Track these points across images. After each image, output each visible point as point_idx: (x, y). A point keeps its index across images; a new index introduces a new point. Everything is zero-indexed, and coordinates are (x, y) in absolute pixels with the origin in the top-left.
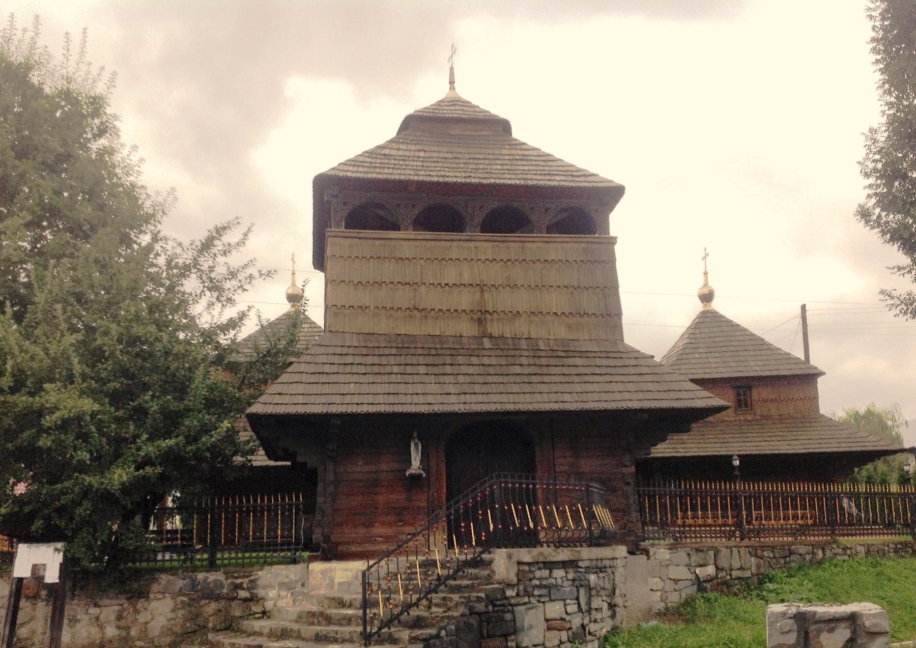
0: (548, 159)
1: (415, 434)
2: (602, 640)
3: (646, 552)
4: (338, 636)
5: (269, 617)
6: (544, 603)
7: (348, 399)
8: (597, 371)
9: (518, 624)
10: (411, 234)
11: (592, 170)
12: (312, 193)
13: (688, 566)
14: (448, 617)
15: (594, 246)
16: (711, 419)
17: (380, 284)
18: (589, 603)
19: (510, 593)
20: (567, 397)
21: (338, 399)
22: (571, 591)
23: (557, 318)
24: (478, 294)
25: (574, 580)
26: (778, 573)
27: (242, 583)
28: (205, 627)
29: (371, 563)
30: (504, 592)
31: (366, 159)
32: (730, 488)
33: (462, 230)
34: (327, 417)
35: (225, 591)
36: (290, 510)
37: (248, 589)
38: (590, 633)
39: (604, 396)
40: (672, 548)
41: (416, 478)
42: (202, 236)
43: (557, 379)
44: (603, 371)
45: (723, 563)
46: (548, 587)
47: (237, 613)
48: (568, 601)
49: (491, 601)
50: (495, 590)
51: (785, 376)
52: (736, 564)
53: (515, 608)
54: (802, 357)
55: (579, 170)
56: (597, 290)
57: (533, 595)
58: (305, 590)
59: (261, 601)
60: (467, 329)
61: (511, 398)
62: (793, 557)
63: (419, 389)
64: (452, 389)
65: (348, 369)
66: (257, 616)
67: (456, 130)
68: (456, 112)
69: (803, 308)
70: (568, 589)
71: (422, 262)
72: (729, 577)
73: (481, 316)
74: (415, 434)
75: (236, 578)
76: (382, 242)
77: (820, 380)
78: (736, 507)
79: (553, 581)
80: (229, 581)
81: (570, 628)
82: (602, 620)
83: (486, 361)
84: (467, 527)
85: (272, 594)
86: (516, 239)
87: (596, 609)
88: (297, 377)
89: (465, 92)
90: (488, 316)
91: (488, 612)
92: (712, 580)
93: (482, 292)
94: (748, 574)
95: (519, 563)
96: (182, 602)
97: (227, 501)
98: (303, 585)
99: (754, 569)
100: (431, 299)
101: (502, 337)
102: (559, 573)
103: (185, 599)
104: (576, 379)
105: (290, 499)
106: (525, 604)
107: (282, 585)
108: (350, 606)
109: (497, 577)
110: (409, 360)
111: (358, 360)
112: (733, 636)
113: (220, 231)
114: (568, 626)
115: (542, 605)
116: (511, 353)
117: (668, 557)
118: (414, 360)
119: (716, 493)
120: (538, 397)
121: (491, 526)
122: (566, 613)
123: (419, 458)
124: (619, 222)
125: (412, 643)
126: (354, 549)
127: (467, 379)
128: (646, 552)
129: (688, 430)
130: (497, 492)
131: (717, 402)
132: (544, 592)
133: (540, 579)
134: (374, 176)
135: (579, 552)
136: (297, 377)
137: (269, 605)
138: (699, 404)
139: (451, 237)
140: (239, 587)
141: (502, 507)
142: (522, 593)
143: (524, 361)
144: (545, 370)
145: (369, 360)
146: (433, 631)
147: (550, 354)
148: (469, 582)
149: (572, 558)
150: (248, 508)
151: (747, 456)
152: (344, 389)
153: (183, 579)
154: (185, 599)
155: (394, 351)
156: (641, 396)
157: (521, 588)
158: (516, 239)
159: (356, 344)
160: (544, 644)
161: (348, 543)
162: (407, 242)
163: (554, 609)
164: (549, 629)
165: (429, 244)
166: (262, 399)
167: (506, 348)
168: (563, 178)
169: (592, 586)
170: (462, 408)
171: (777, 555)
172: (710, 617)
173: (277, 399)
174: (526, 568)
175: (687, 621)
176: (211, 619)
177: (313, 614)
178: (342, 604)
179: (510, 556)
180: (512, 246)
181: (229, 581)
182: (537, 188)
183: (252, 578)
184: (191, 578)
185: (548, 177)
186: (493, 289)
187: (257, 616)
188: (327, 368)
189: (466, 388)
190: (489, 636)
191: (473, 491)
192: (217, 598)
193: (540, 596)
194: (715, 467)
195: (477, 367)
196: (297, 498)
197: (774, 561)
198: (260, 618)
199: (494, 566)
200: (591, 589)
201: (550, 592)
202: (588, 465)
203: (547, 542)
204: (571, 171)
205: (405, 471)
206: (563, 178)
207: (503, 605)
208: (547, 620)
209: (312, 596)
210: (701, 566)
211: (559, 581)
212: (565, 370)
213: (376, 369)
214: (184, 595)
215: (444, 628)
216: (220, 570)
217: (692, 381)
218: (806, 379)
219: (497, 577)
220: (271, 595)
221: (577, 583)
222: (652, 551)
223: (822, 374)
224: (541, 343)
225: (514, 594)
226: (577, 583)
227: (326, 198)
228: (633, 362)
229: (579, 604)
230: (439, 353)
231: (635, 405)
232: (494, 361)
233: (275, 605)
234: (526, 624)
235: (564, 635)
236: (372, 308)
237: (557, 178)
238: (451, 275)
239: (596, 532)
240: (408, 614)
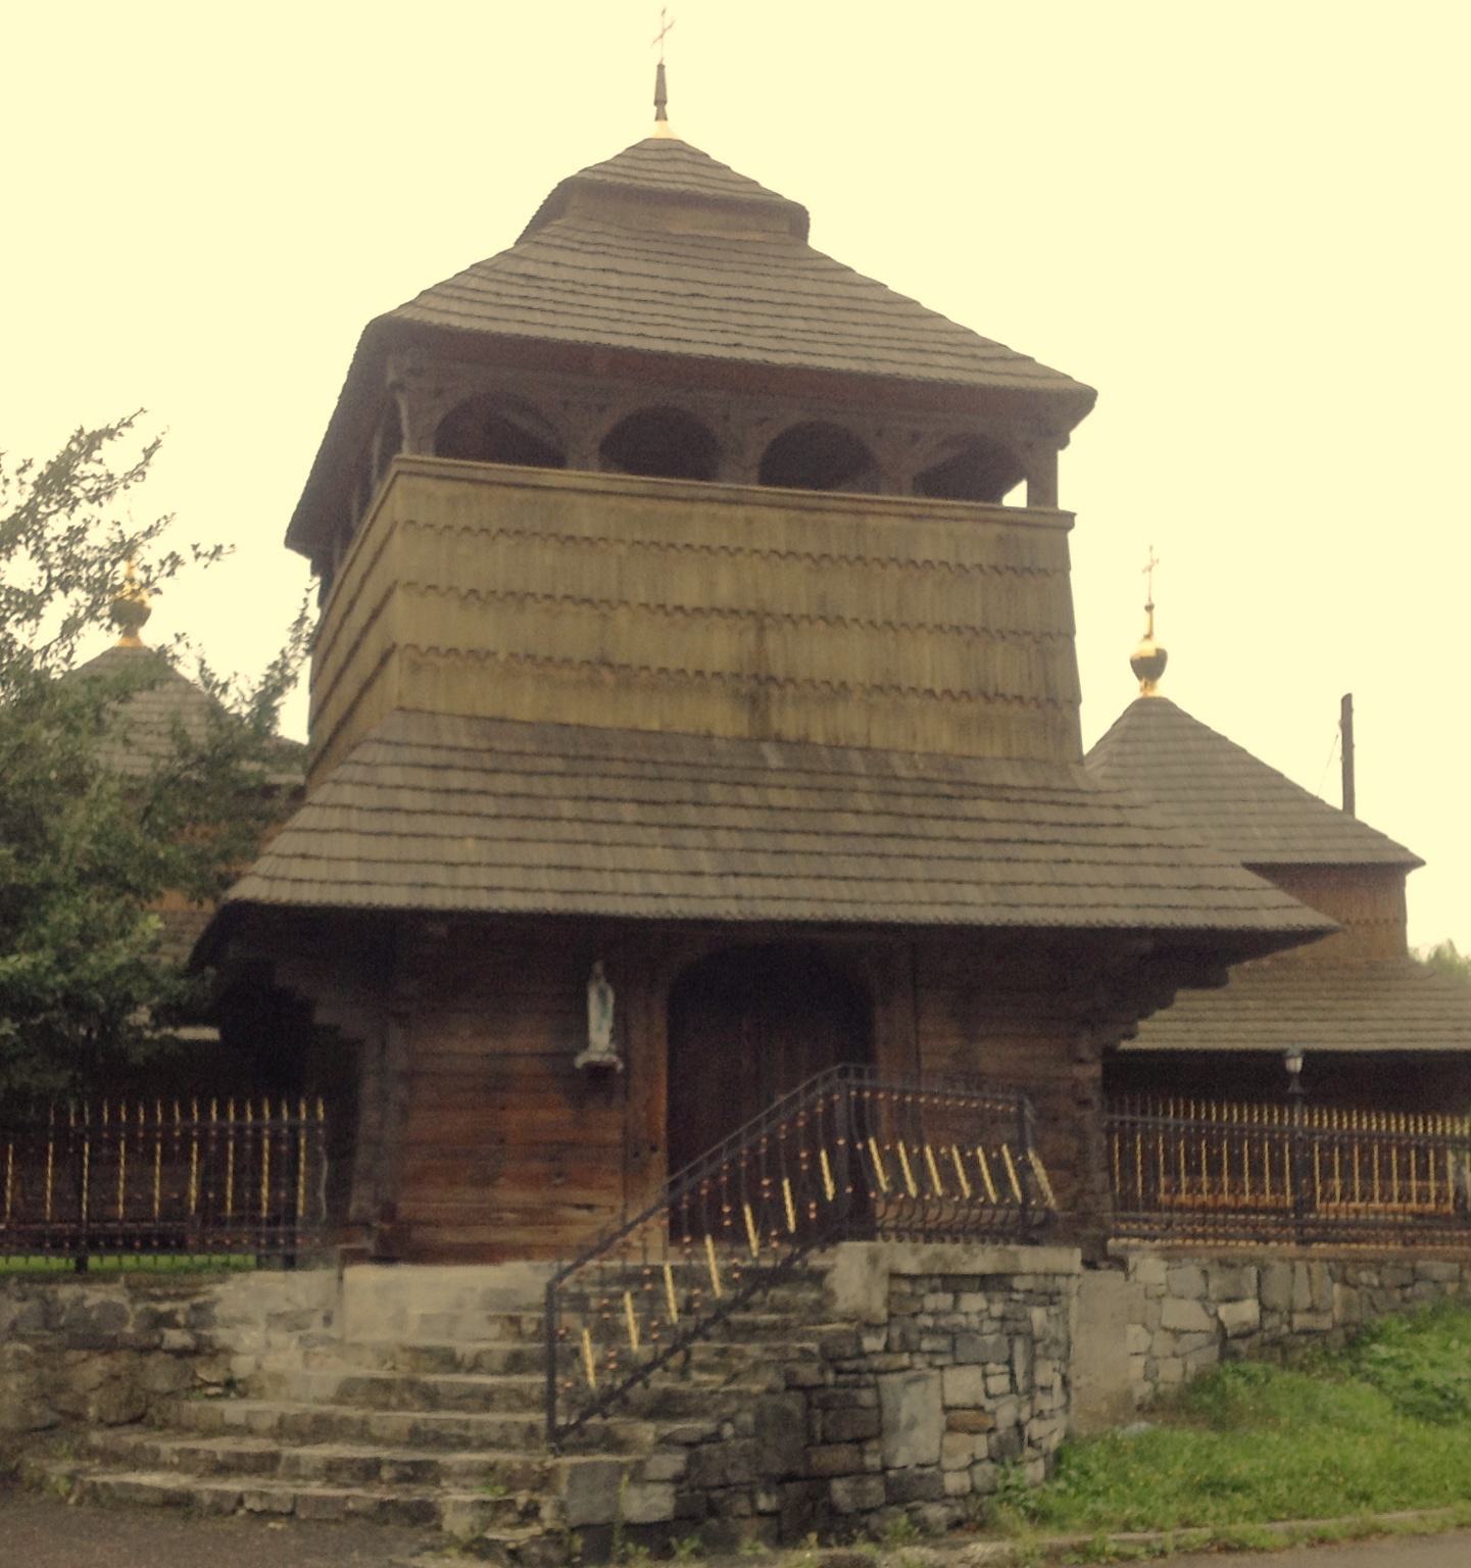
0: (906, 311)
1: (598, 967)
2: (1051, 1459)
3: (1120, 1263)
4: (471, 1433)
5: (243, 1395)
6: (941, 1368)
7: (465, 876)
8: (1033, 833)
9: (887, 1415)
10: (595, 479)
11: (1018, 347)
13: (1203, 1299)
14: (739, 1394)
15: (1022, 532)
16: (1286, 954)
17: (520, 598)
18: (1030, 1373)
19: (871, 1343)
20: (970, 893)
21: (440, 875)
22: (997, 1344)
23: (934, 702)
24: (751, 637)
25: (1003, 1319)
26: (1396, 1326)
27: (171, 1314)
28: (78, 1417)
29: (567, 1263)
30: (859, 1343)
31: (485, 285)
32: (1340, 1124)
33: (704, 474)
34: (421, 915)
35: (129, 1329)
36: (222, 1142)
37: (190, 1327)
38: (1031, 1443)
39: (1055, 895)
40: (1170, 1256)
41: (599, 1073)
42: (46, 451)
43: (944, 848)
44: (1049, 833)
45: (1276, 1297)
46: (952, 1334)
47: (162, 1384)
48: (991, 1367)
49: (832, 1360)
50: (840, 1335)
51: (1334, 866)
52: (1303, 1300)
53: (882, 1379)
54: (1335, 800)
56: (1027, 640)
57: (919, 1350)
58: (333, 1332)
59: (222, 1357)
60: (722, 718)
61: (844, 890)
62: (1421, 1287)
63: (629, 858)
64: (705, 861)
65: (456, 803)
66: (212, 1391)
67: (683, 224)
70: (991, 1339)
71: (622, 549)
72: (1285, 1329)
73: (757, 688)
74: (598, 967)
76: (528, 494)
78: (1303, 1169)
79: (961, 1319)
80: (140, 1307)
81: (992, 1430)
83: (775, 797)
84: (777, 1188)
86: (845, 505)
87: (1043, 1389)
88: (335, 819)
89: (688, 127)
90: (775, 691)
91: (823, 1386)
92: (1250, 1334)
93: (761, 629)
94: (1325, 1323)
95: (895, 1276)
96: (18, 1355)
97: (132, 1112)
98: (327, 1320)
99: (1338, 1313)
100: (641, 642)
101: (804, 742)
102: (973, 1302)
103: (26, 1348)
104: (987, 851)
106: (903, 1369)
107: (275, 1319)
108: (476, 1366)
109: (841, 1306)
110: (597, 787)
111: (476, 781)
112: (1336, 1458)
113: (89, 443)
115: (935, 1373)
116: (828, 780)
117: (1162, 1277)
118: (612, 787)
119: (1282, 1133)
120: (906, 891)
122: (988, 1396)
123: (607, 1024)
124: (1081, 468)
125: (664, 1451)
126: (449, 1237)
127: (738, 841)
128: (1120, 1263)
129: (1219, 982)
130: (840, 1112)
131: (1306, 917)
132: (942, 1343)
133: (934, 1314)
135: (1015, 1254)
136: (335, 819)
137: (242, 1366)
138: (1270, 920)
139: (693, 492)
140: (167, 1320)
141: (851, 1144)
142: (896, 1345)
143: (864, 802)
144: (915, 827)
145: (502, 783)
146: (705, 1426)
147: (921, 787)
148: (774, 1317)
149: (1001, 1268)
150: (222, 1131)
151: (1325, 1054)
152: (453, 851)
153: (18, 1299)
154: (26, 1348)
155: (558, 764)
156: (1139, 896)
157: (896, 1332)
158: (845, 505)
159: (465, 742)
161: (437, 1224)
162: (585, 499)
163: (962, 1385)
164: (951, 1428)
165: (638, 506)
166: (264, 865)
167: (822, 769)
168: (956, 362)
169: (1037, 1332)
170: (729, 910)
171: (1388, 1282)
172: (1268, 1417)
173: (298, 869)
174: (906, 1287)
175: (1218, 1424)
176: (93, 1397)
177: (387, 1386)
178: (449, 1361)
179: (873, 1260)
180: (838, 520)
181: (140, 1307)
182: (895, 381)
183: (199, 1300)
184: (41, 1296)
185: (922, 358)
186: (788, 626)
187: (212, 1391)
188: (406, 799)
189: (739, 863)
190: (826, 1442)
192: (109, 1347)
193: (933, 1352)
194: (1250, 1076)
195: (756, 813)
197: (1381, 1293)
198: (217, 1396)
199: (834, 1281)
200: (1034, 1342)
201: (956, 1345)
202: (996, 1055)
203: (896, 1229)
204: (964, 341)
205: (576, 1054)
206: (956, 362)
207: (856, 1371)
208: (947, 1409)
209: (357, 1346)
210: (1229, 1300)
211: (974, 1320)
212: (963, 830)
213: (521, 806)
214: (23, 1338)
215: (729, 1420)
216: (116, 1281)
217: (1250, 866)
219: (841, 1306)
220: (247, 1342)
221: (1011, 1325)
222: (1132, 1260)
223: (1418, 863)
224: (895, 760)
226: (1011, 1325)
228: (1111, 816)
229: (1012, 1375)
230: (670, 778)
231: (1128, 918)
232: (793, 799)
233: (259, 1367)
234: (904, 1417)
235: (981, 1445)
236: (502, 656)
237: (943, 361)
238: (688, 588)
239: (1039, 1216)
240: (646, 1385)
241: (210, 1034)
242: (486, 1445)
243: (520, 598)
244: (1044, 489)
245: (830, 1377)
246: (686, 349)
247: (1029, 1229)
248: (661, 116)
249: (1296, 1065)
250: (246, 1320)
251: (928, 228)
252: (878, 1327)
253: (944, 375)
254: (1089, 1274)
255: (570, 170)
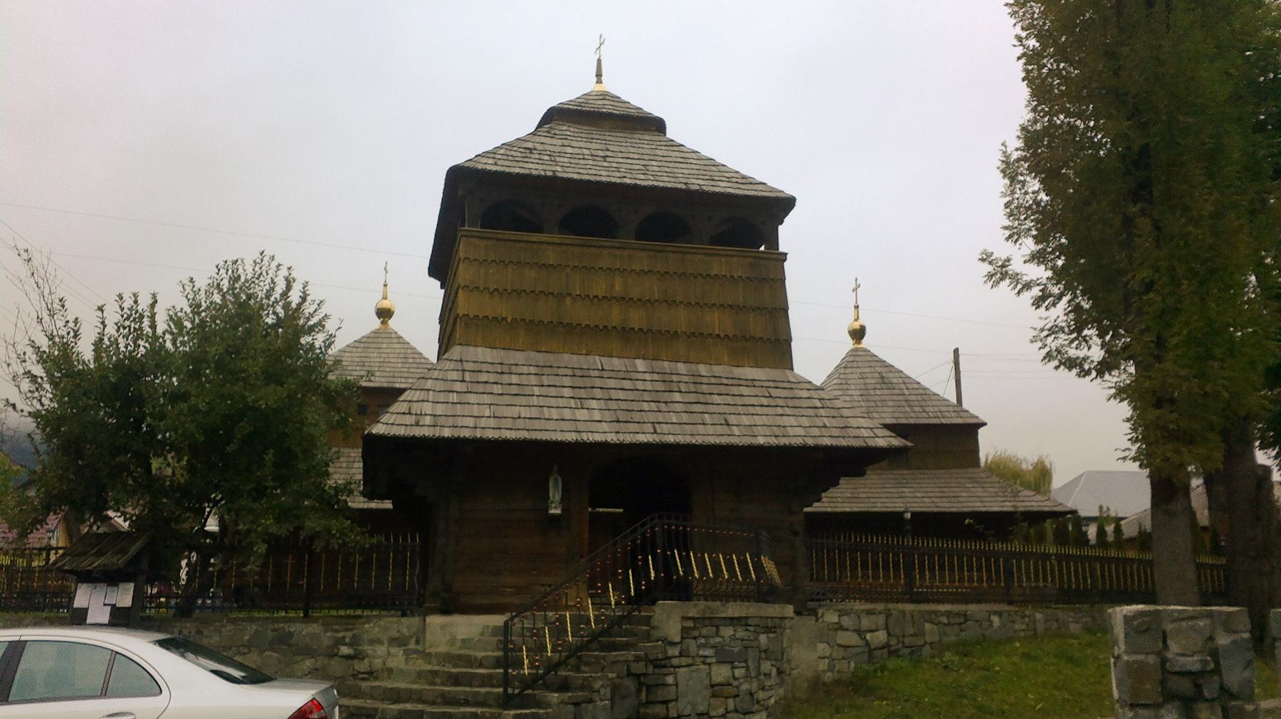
1: (555, 468)
10: (557, 238)
11: (760, 179)
12: (442, 187)
15: (762, 262)
17: (519, 293)
27: (344, 638)
30: (666, 652)
37: (350, 645)
38: (758, 702)
49: (651, 661)
54: (954, 400)
55: (744, 177)
58: (420, 648)
68: (607, 108)
69: (956, 351)
74: (555, 468)
75: (337, 631)
76: (523, 245)
77: (981, 431)
82: (771, 688)
85: (381, 650)
89: (609, 85)
98: (417, 642)
105: (405, 539)
111: (492, 378)
114: (734, 691)
118: (557, 381)
121: (653, 575)
126: (479, 601)
128: (813, 612)
129: (861, 474)
134: (517, 170)
143: (683, 387)
160: (707, 714)
164: (714, 696)
165: (576, 250)
166: (385, 418)
174: (690, 624)
181: (329, 634)
191: (632, 532)
196: (413, 539)
204: (773, 190)
218: (970, 430)
220: (379, 652)
225: (677, 653)
227: (460, 193)
232: (649, 386)
239: (766, 588)
241: (388, 505)
242: (478, 704)
243: (519, 293)
244: (773, 241)
245: (651, 669)
246: (598, 179)
247: (766, 594)
248: (599, 82)
249: (908, 516)
250: (379, 642)
251: (720, 128)
252: (676, 644)
253: (722, 190)
254: (798, 617)
255: (554, 103)
